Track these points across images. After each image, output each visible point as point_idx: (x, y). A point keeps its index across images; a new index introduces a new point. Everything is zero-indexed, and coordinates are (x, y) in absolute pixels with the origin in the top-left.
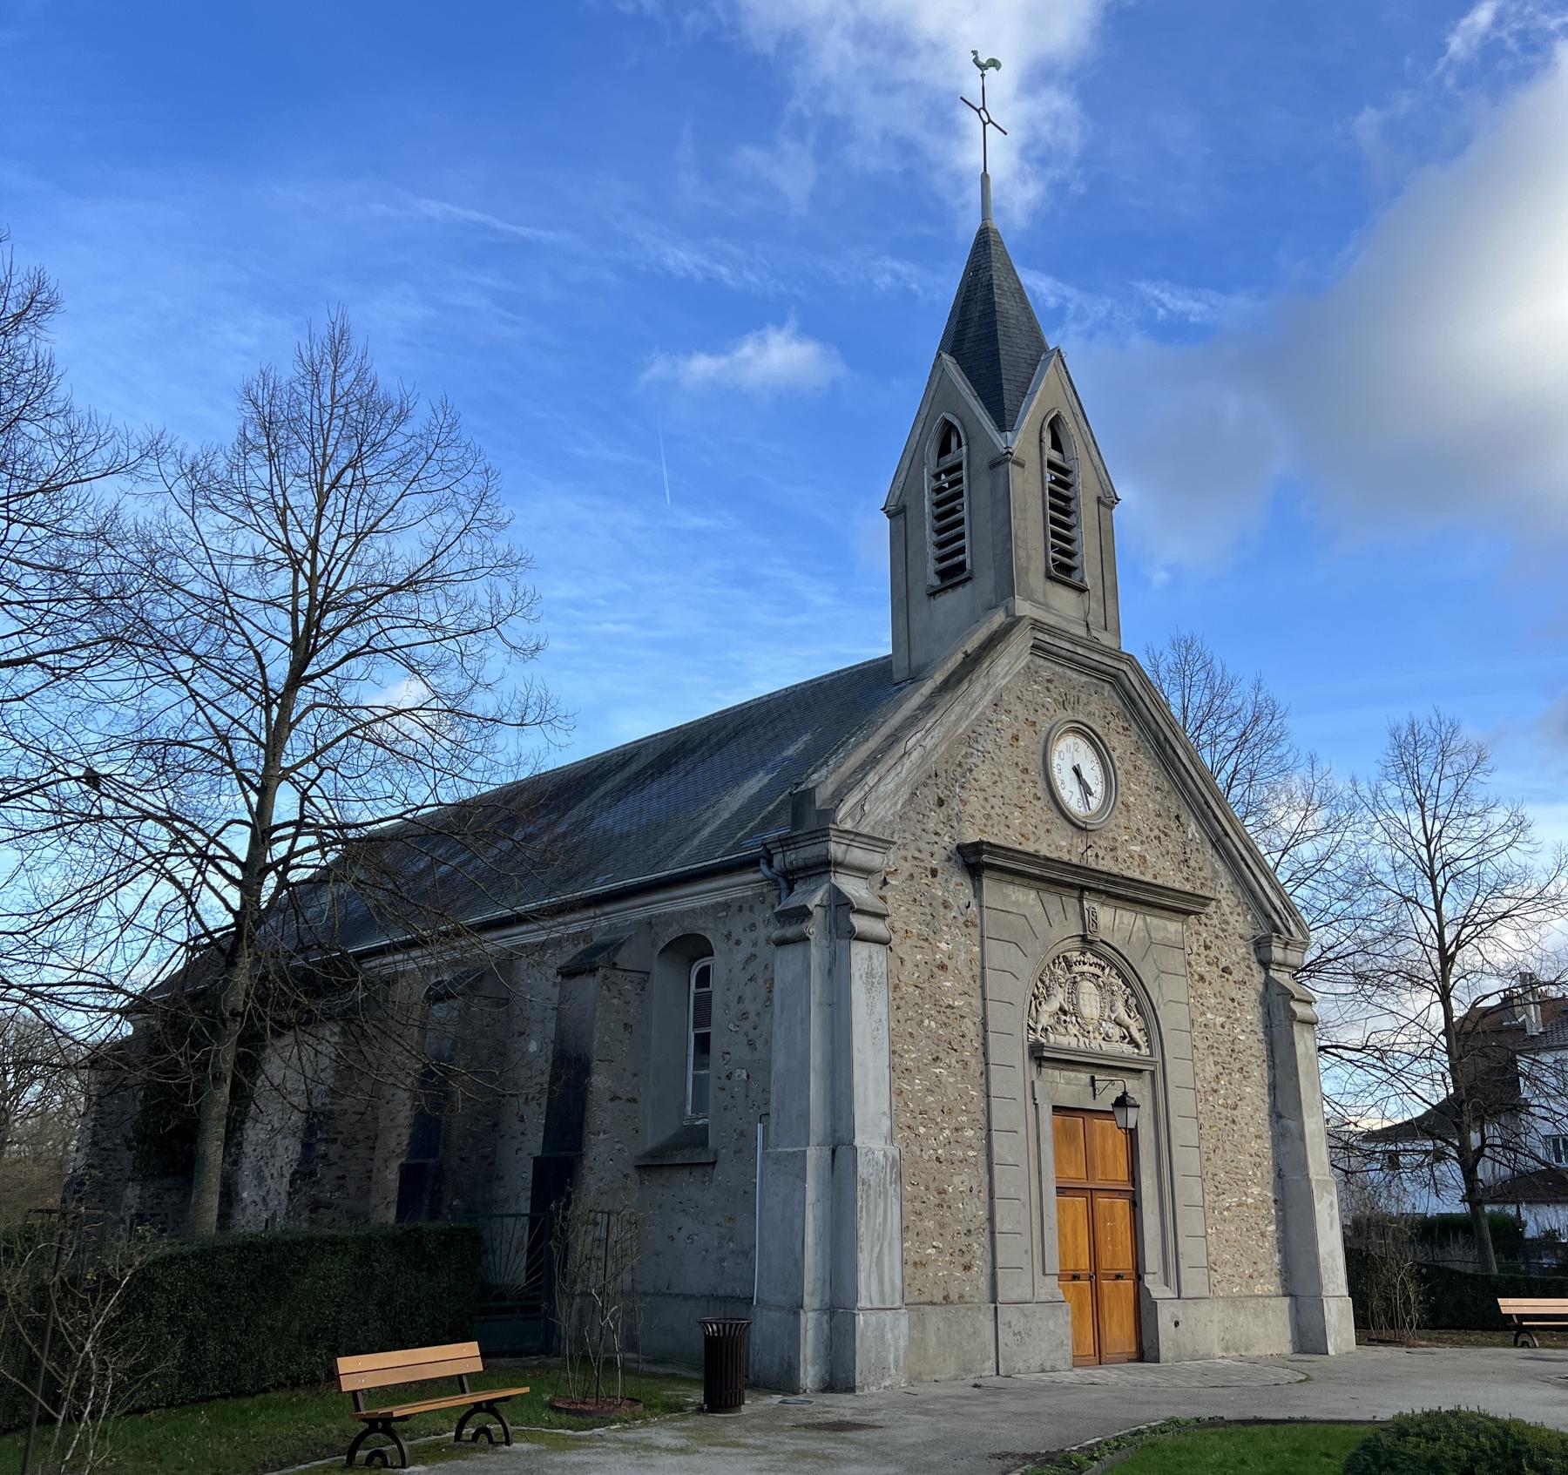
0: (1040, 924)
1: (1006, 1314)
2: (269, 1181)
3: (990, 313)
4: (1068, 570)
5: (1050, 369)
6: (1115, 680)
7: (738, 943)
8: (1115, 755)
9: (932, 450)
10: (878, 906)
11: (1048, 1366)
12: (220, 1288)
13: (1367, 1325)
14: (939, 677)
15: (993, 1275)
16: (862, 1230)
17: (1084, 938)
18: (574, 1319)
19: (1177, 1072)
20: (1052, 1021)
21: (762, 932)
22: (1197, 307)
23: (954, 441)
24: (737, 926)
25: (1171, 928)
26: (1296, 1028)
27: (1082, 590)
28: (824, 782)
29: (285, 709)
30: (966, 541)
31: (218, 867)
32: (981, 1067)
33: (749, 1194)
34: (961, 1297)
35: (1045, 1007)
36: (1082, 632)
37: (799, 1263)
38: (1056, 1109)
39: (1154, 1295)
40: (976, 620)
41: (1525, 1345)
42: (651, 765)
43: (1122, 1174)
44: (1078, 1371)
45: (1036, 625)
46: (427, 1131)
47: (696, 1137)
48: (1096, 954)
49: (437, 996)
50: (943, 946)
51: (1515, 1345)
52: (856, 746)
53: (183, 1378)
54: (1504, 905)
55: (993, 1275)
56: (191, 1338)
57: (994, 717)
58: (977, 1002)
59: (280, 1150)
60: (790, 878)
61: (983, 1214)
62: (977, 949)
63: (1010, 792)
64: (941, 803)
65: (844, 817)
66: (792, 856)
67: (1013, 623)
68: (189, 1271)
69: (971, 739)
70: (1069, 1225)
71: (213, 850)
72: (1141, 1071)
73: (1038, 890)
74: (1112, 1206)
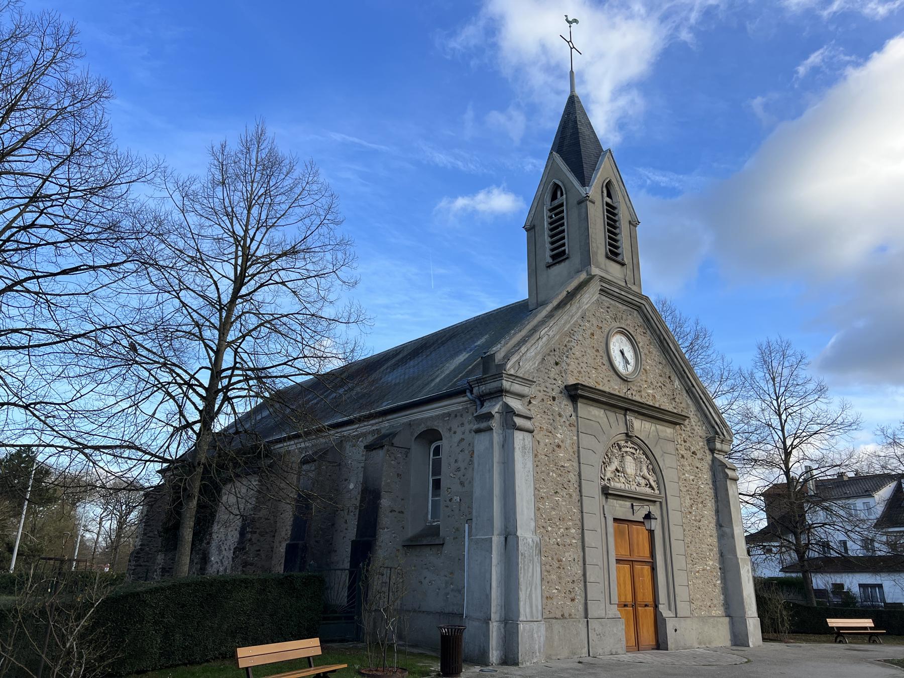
0: (606, 427)
1: (593, 624)
2: (224, 552)
3: (576, 133)
4: (617, 255)
5: (606, 159)
6: (639, 308)
7: (455, 433)
8: (640, 345)
9: (548, 197)
10: (528, 413)
11: (614, 651)
12: (183, 606)
13: (770, 631)
14: (555, 303)
15: (586, 604)
16: (521, 580)
17: (627, 434)
18: (372, 623)
19: (673, 503)
20: (612, 476)
21: (467, 427)
22: (664, 179)
23: (559, 193)
24: (454, 424)
25: (668, 431)
26: (728, 482)
27: (623, 264)
28: (499, 351)
29: (230, 312)
30: (566, 241)
31: (195, 391)
32: (578, 497)
33: (461, 560)
34: (570, 615)
35: (609, 468)
36: (624, 284)
37: (488, 597)
38: (615, 520)
39: (664, 615)
40: (571, 277)
41: (840, 642)
42: (409, 354)
43: (647, 553)
44: (629, 654)
45: (602, 279)
46: (300, 526)
47: (434, 531)
48: (633, 443)
49: (305, 462)
50: (559, 435)
51: (836, 642)
52: (514, 334)
53: (161, 655)
54: (816, 428)
55: (586, 604)
56: (167, 633)
57: (582, 324)
58: (576, 464)
59: (230, 537)
60: (482, 399)
61: (580, 572)
62: (575, 438)
63: (590, 361)
64: (557, 364)
65: (510, 368)
66: (483, 388)
67: (591, 278)
68: (166, 596)
69: (571, 333)
70: (622, 579)
71: (193, 382)
72: (655, 501)
73: (605, 410)
74: (642, 569)
